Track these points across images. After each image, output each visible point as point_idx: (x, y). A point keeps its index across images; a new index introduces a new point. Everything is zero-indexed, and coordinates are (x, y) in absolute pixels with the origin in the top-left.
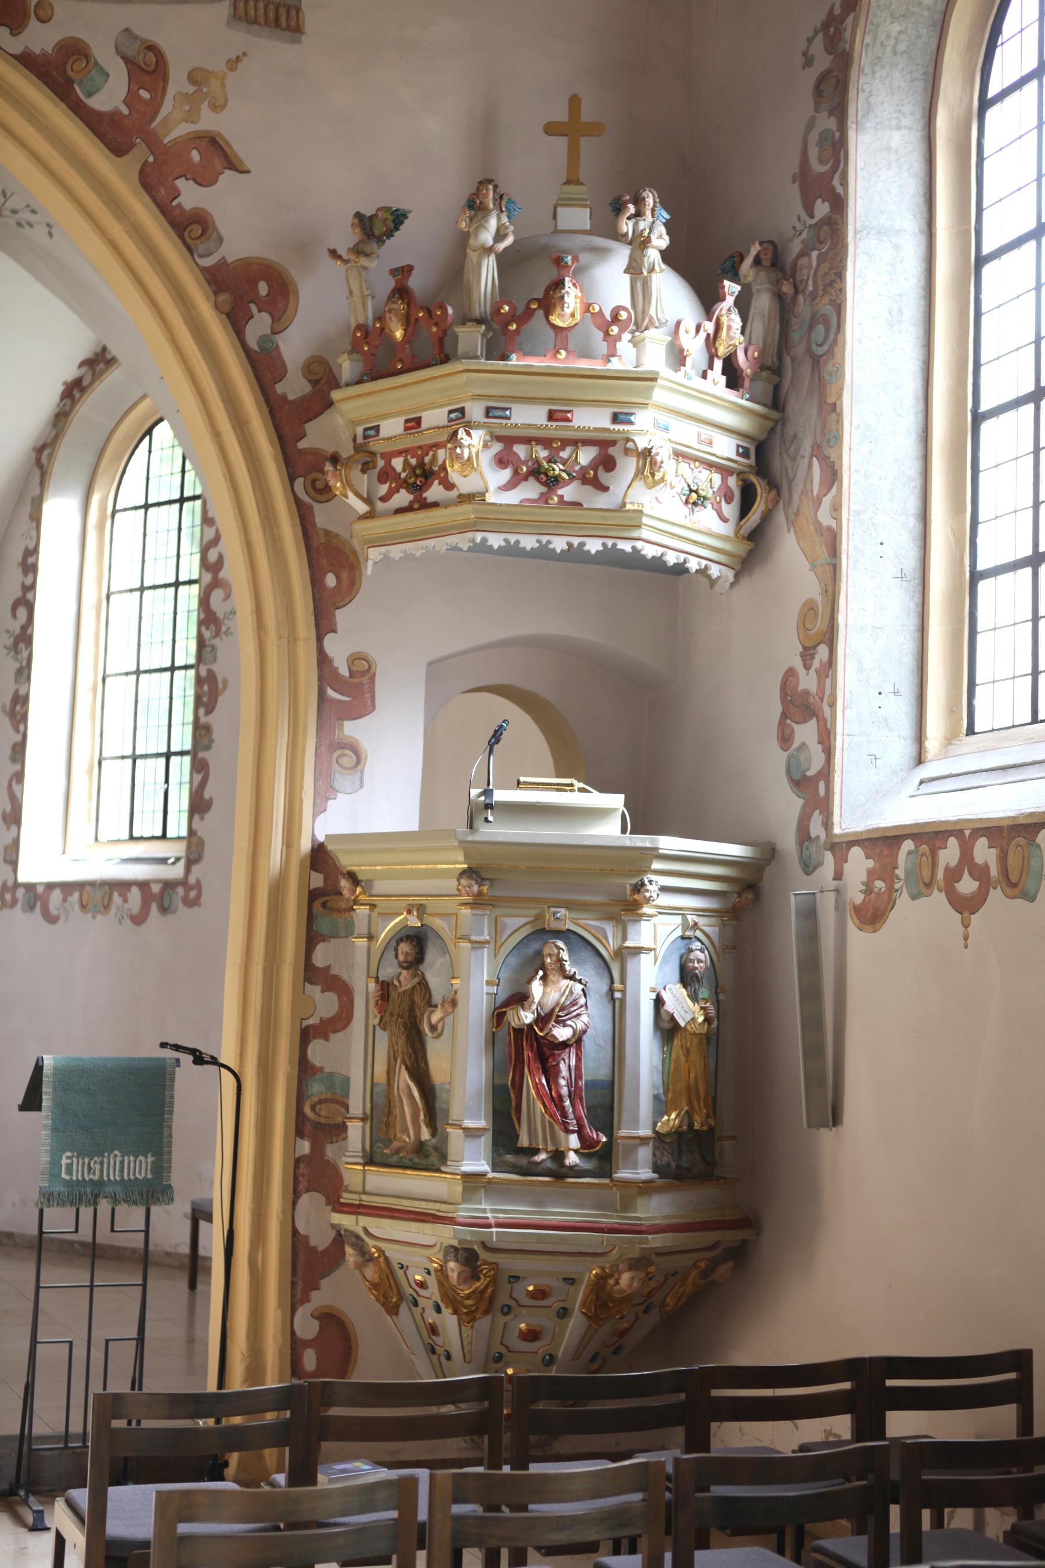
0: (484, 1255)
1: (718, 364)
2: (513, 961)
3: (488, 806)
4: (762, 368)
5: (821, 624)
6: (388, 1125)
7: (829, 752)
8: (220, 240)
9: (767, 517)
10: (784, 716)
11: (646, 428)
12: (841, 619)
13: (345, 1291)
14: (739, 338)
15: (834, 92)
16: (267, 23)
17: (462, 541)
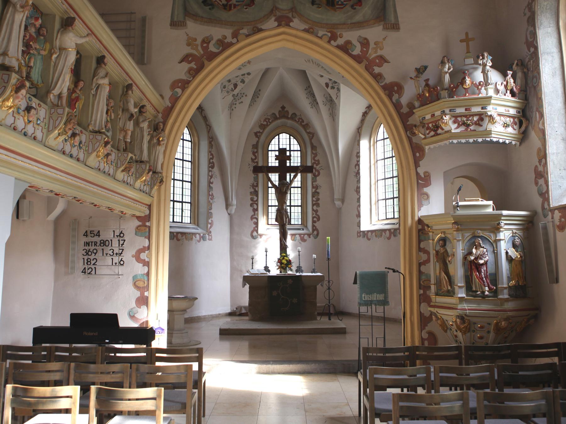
0: (466, 317)
1: (508, 92)
2: (468, 244)
3: (458, 206)
4: (521, 91)
5: (542, 154)
6: (440, 286)
7: (547, 186)
8: (385, 79)
9: (527, 128)
10: (536, 178)
11: (491, 110)
12: (547, 152)
13: (434, 327)
14: (513, 84)
15: (532, 22)
16: (391, 28)
17: (447, 142)
